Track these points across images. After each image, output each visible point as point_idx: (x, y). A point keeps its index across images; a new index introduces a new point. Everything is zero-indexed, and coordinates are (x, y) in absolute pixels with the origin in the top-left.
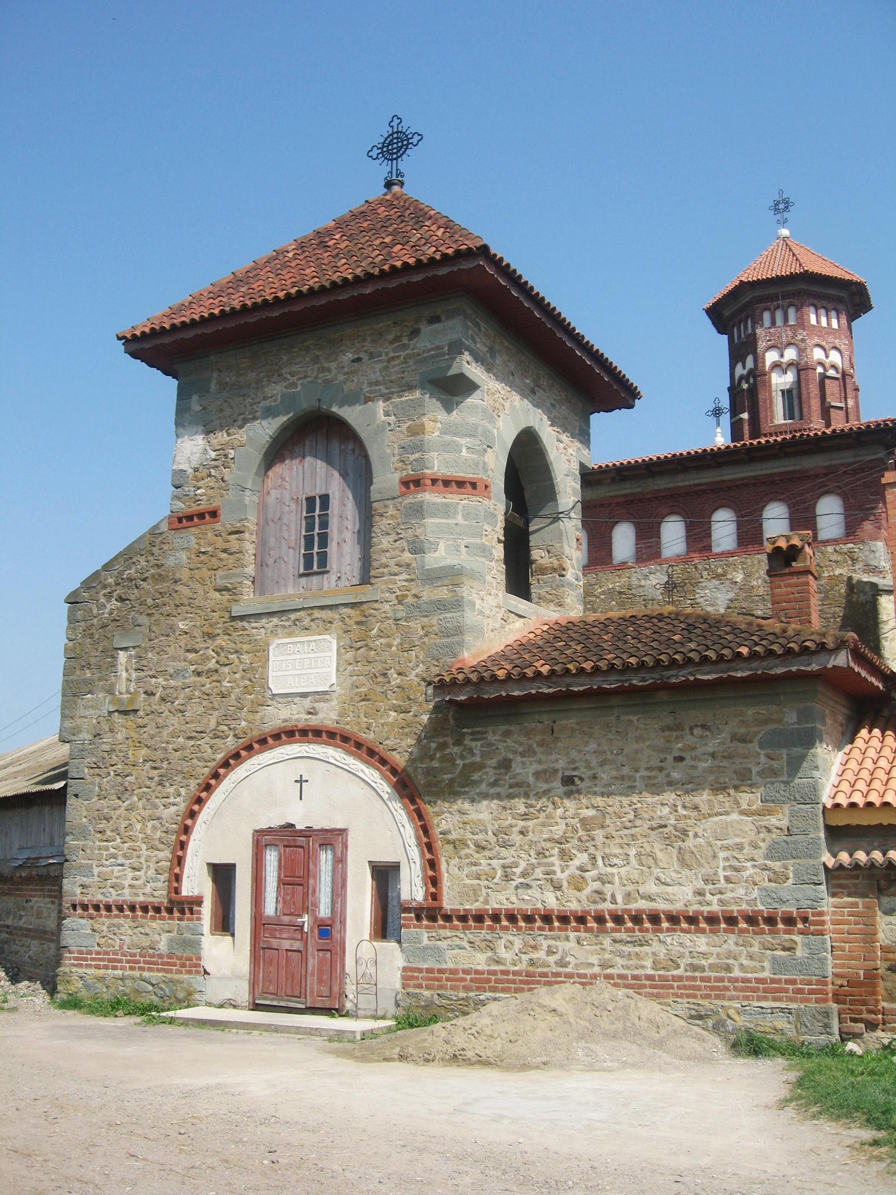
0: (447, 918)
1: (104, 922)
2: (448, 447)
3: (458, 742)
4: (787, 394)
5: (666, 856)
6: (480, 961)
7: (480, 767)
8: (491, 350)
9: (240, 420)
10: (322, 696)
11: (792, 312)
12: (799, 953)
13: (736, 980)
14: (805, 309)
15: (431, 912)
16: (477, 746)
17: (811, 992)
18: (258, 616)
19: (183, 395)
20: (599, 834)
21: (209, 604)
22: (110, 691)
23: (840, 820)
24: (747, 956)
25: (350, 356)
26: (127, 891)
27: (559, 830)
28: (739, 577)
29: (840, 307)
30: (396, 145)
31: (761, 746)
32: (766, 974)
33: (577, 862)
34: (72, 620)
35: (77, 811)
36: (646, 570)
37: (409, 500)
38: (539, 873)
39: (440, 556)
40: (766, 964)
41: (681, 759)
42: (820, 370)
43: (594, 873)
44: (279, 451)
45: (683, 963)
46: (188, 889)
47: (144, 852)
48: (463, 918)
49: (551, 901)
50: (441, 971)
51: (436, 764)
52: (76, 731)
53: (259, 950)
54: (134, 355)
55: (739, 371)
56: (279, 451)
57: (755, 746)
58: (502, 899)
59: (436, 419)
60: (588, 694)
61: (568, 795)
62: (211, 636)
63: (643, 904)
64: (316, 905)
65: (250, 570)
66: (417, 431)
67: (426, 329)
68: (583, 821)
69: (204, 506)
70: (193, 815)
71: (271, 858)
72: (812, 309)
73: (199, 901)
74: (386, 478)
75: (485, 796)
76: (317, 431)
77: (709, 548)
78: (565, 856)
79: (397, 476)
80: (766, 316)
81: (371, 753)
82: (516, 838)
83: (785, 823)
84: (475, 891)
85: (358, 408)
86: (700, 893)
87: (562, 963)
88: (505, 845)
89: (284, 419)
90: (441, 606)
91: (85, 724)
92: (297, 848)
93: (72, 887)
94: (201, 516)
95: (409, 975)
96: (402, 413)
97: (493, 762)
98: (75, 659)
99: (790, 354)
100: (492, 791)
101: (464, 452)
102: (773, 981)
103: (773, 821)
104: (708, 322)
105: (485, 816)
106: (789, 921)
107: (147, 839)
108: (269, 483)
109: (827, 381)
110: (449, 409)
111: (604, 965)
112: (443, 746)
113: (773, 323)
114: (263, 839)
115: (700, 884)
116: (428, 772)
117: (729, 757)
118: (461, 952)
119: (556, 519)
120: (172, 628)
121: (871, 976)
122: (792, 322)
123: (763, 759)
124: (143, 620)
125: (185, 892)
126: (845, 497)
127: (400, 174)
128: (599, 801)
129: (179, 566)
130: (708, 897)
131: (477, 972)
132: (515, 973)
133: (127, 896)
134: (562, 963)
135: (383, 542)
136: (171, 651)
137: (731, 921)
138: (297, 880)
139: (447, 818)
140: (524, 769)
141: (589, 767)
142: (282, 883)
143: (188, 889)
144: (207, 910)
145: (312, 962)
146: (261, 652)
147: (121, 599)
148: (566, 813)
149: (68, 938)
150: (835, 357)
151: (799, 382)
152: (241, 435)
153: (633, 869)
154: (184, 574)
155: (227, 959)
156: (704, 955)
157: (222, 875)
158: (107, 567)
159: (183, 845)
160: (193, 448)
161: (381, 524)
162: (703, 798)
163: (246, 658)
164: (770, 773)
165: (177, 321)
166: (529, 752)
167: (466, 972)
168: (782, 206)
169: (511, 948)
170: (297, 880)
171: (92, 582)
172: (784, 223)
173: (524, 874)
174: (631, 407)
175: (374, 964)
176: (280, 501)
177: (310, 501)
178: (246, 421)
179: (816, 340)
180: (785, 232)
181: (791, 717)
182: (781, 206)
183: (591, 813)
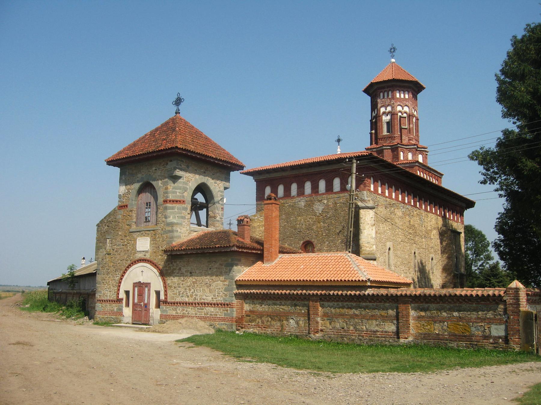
0: (169, 303)
3: (172, 263)
4: (388, 123)
7: (175, 269)
10: (147, 252)
11: (390, 93)
14: (394, 92)
25: (154, 168)
28: (325, 202)
30: (178, 102)
32: (223, 316)
41: (210, 269)
42: (400, 114)
57: (223, 267)
58: (178, 299)
62: (126, 236)
66: (167, 189)
67: (169, 163)
73: (122, 299)
77: (318, 192)
79: (162, 200)
80: (381, 94)
86: (212, 298)
88: (179, 287)
97: (177, 268)
99: (389, 109)
103: (226, 283)
112: (169, 264)
113: (384, 97)
137: (218, 305)
150: (406, 109)
155: (127, 312)
172: (393, 57)
179: (399, 103)
180: (393, 60)
182: (392, 50)
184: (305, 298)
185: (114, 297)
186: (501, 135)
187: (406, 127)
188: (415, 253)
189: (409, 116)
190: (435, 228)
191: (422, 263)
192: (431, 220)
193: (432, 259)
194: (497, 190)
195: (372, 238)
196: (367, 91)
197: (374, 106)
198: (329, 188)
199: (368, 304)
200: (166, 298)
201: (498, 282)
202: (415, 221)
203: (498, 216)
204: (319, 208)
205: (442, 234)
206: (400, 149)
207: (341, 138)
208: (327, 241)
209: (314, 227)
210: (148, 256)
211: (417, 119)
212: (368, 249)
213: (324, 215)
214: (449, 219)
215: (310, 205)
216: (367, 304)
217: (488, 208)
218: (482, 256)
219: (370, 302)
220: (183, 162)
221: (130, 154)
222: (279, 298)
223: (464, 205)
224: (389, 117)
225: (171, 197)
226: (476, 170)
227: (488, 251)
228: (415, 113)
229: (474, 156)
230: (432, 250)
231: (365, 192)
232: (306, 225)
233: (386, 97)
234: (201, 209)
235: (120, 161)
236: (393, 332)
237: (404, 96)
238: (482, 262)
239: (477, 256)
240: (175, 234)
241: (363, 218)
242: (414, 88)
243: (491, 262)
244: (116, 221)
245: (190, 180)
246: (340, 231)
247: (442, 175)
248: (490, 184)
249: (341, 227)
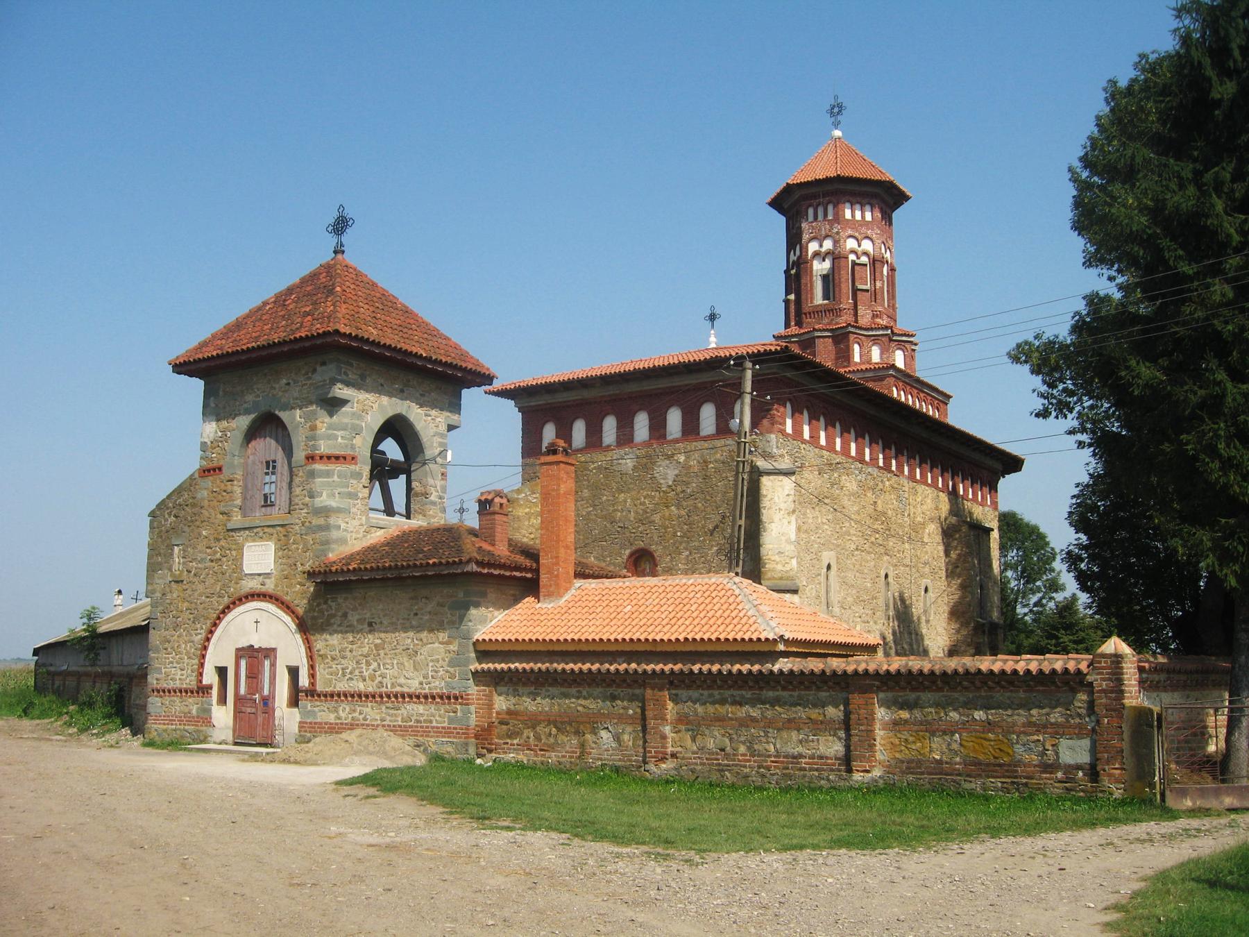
0: (319, 696)
1: (167, 700)
2: (329, 437)
3: (326, 603)
4: (825, 278)
5: (408, 664)
6: (331, 718)
7: (334, 616)
9: (232, 415)
10: (267, 575)
11: (830, 208)
12: (459, 714)
14: (840, 206)
15: (312, 693)
16: (333, 604)
18: (240, 529)
19: (207, 394)
20: (382, 652)
21: (217, 521)
22: (170, 569)
23: (482, 648)
24: (438, 715)
27: (366, 650)
28: (682, 458)
29: (874, 201)
30: (340, 225)
32: (446, 725)
34: (152, 527)
35: (154, 637)
36: (622, 452)
37: (308, 468)
38: (357, 672)
39: (324, 500)
41: (416, 614)
42: (852, 257)
44: (252, 434)
46: (206, 681)
47: (186, 660)
48: (325, 696)
49: (361, 687)
52: (153, 592)
53: (238, 712)
54: (179, 373)
55: (793, 258)
56: (252, 434)
58: (342, 686)
59: (324, 422)
60: (370, 580)
61: (370, 632)
62: (218, 540)
63: (398, 689)
64: (262, 689)
65: (239, 502)
66: (313, 428)
67: (319, 369)
68: (376, 646)
69: (215, 464)
70: (208, 640)
71: (243, 663)
72: (848, 205)
73: (210, 687)
74: (299, 455)
75: (336, 632)
76: (268, 425)
77: (664, 436)
78: (368, 664)
80: (811, 211)
81: (288, 608)
82: (348, 653)
83: (456, 649)
84: (330, 681)
85: (287, 413)
86: (421, 683)
87: (365, 719)
88: (344, 658)
89: (253, 416)
90: (322, 528)
91: (158, 588)
92: (255, 657)
93: (152, 680)
94: (214, 470)
95: (302, 725)
96: (310, 417)
98: (153, 550)
99: (828, 245)
103: (451, 647)
105: (335, 642)
106: (456, 698)
107: (187, 653)
108: (249, 451)
109: (857, 268)
110: (331, 415)
111: (382, 720)
112: (318, 605)
113: (816, 218)
114: (241, 653)
116: (314, 618)
118: (324, 713)
119: (425, 464)
120: (200, 534)
121: (491, 725)
122: (830, 218)
124: (186, 529)
125: (204, 683)
127: (342, 245)
128: (383, 635)
129: (203, 499)
133: (178, 684)
134: (365, 719)
135: (298, 491)
136: (199, 547)
137: (433, 698)
138: (254, 675)
139: (320, 643)
140: (353, 618)
142: (247, 677)
143: (206, 681)
144: (215, 692)
145: (260, 720)
146: (240, 549)
147: (176, 516)
148: (371, 640)
149: (151, 709)
150: (867, 245)
151: (833, 268)
152: (234, 424)
153: (394, 672)
154: (206, 503)
155: (223, 717)
157: (222, 672)
158: (169, 497)
159: (203, 656)
160: (211, 429)
161: (297, 480)
162: (424, 635)
163: (234, 553)
164: (452, 623)
165: (196, 357)
166: (355, 609)
168: (836, 110)
169: (345, 711)
170: (254, 675)
171: (162, 506)
172: (836, 125)
173: (351, 673)
175: (287, 718)
176: (254, 463)
177: (268, 463)
178: (236, 415)
179: (850, 232)
180: (837, 133)
181: (461, 595)
182: (836, 110)
183: (379, 641)
185: (191, 682)
186: (1081, 306)
187: (868, 287)
188: (886, 576)
189: (874, 261)
190: (932, 520)
191: (902, 600)
192: (923, 499)
193: (926, 590)
194: (1072, 432)
195: (789, 542)
196: (777, 203)
197: (794, 239)
198: (691, 427)
200: (313, 684)
201: (1075, 642)
202: (887, 502)
203: (1076, 491)
204: (666, 473)
205: (948, 534)
206: (852, 337)
208: (686, 549)
209: (656, 518)
210: (270, 587)
211: (892, 270)
212: (779, 567)
213: (679, 489)
214: (965, 497)
215: (646, 465)
217: (1051, 478)
218: (1038, 583)
219: (784, 689)
223: (998, 466)
224: (827, 264)
225: (324, 448)
226: (1026, 385)
227: (1053, 570)
228: (888, 255)
229: (1021, 354)
230: (927, 570)
231: (773, 436)
232: (637, 513)
233: (820, 217)
235: (204, 365)
237: (863, 216)
238: (1040, 595)
239: (1027, 582)
240: (335, 534)
241: (769, 497)
242: (886, 197)
243: (1059, 597)
244: (194, 505)
245: (368, 408)
246: (717, 527)
248: (1057, 417)
249: (719, 518)
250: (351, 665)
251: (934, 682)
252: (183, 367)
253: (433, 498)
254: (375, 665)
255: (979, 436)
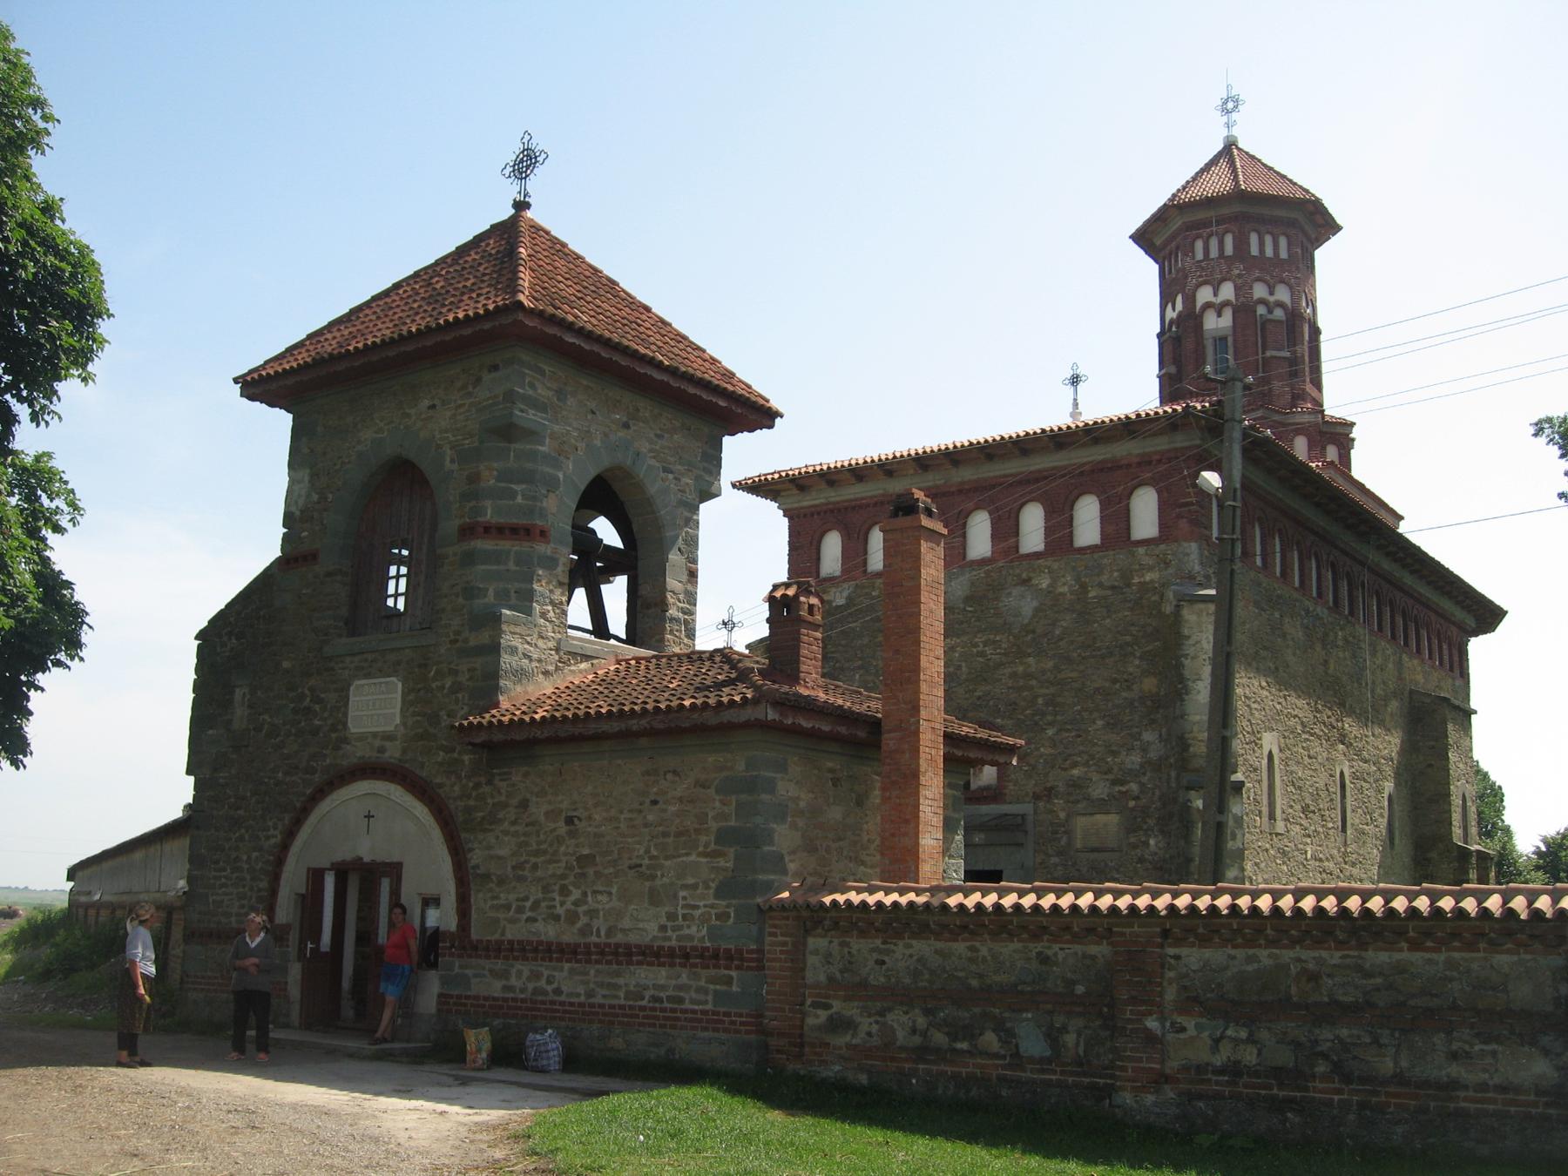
0: (475, 948)
3: (490, 782)
7: (505, 805)
8: (561, 394)
10: (389, 737)
12: (735, 988)
13: (685, 1011)
17: (742, 1024)
25: (427, 403)
26: (233, 919)
31: (717, 792)
32: (709, 1007)
33: (572, 898)
40: (710, 998)
41: (655, 802)
42: (1261, 310)
43: (585, 908)
45: (647, 994)
50: (467, 997)
51: (472, 803)
57: (712, 791)
58: (512, 933)
66: (474, 478)
67: (487, 377)
79: (458, 522)
80: (1199, 245)
86: (663, 928)
88: (521, 879)
97: (514, 802)
100: (513, 829)
101: (519, 499)
102: (714, 1013)
103: (722, 863)
104: (1140, 253)
109: (1269, 326)
112: (477, 785)
115: (663, 921)
117: (691, 802)
123: (717, 804)
126: (1159, 492)
130: (670, 933)
131: (494, 999)
132: (523, 1001)
137: (686, 956)
141: (586, 809)
156: (663, 988)
167: (486, 999)
174: (771, 426)
184: (1091, 930)
196: (1144, 238)
199: (1405, 955)
207: (1081, 371)
210: (393, 753)
216: (1397, 956)
219: (1415, 946)
220: (542, 373)
221: (329, 347)
222: (965, 927)
223: (1471, 622)
225: (489, 515)
234: (608, 574)
235: (290, 381)
236: (1539, 1092)
247: (1402, 518)
250: (536, 893)
251: (1260, 931)
252: (257, 386)
253: (672, 612)
254: (576, 894)
255: (1456, 572)
